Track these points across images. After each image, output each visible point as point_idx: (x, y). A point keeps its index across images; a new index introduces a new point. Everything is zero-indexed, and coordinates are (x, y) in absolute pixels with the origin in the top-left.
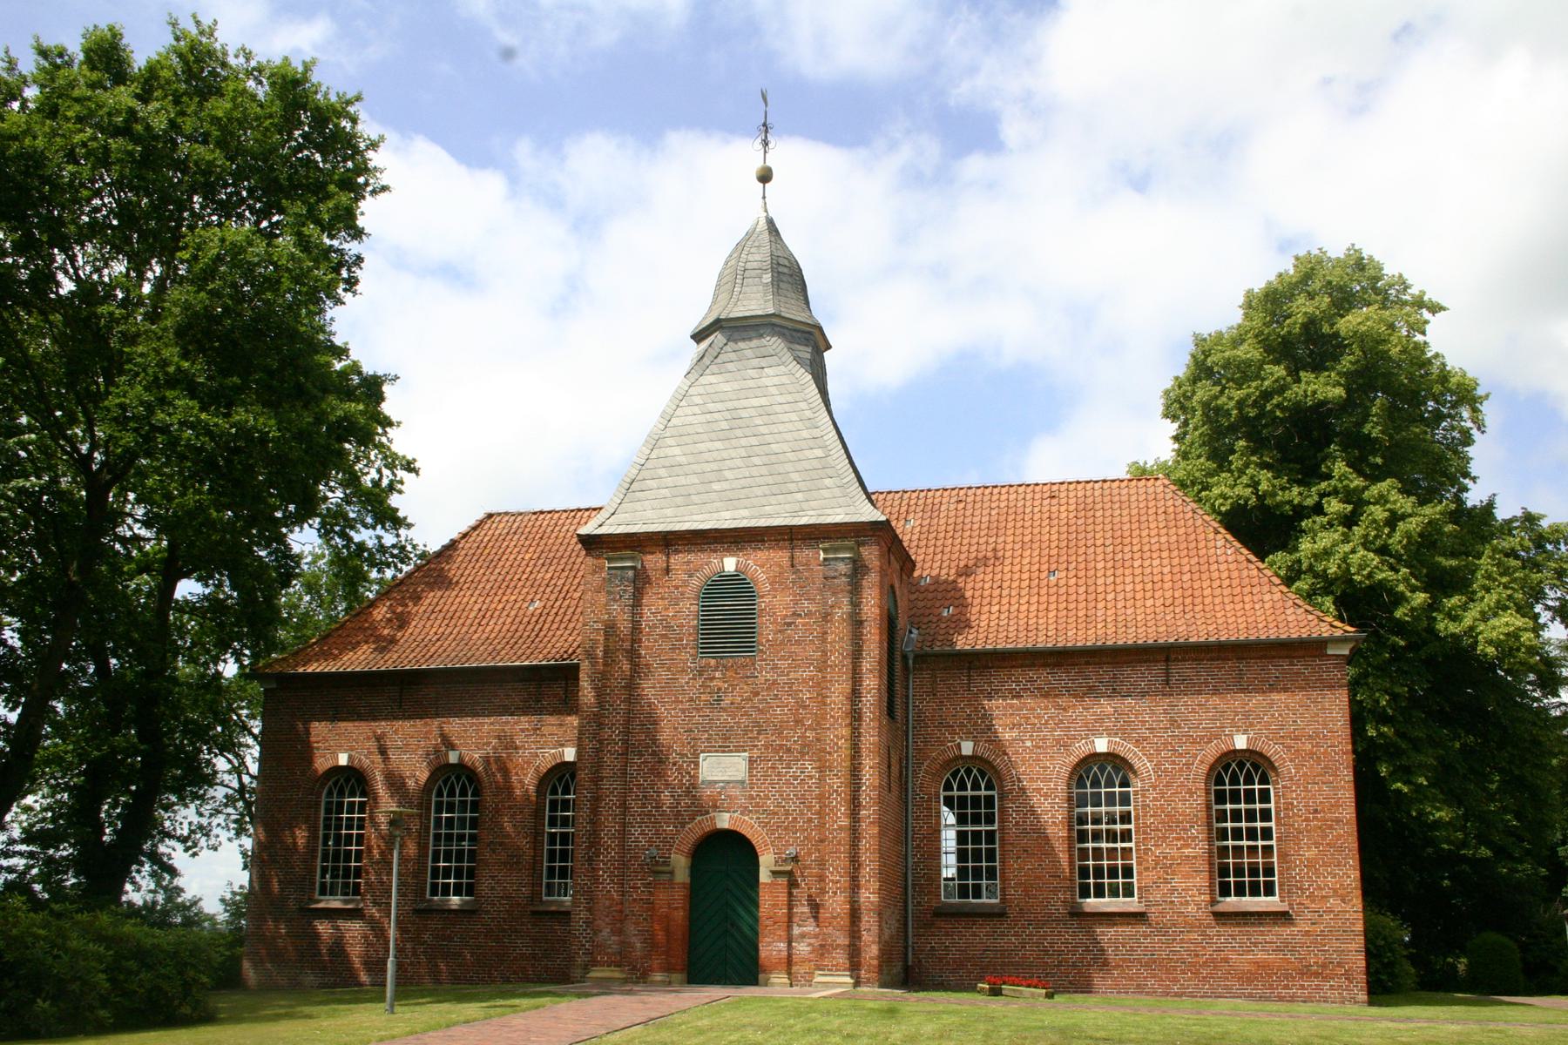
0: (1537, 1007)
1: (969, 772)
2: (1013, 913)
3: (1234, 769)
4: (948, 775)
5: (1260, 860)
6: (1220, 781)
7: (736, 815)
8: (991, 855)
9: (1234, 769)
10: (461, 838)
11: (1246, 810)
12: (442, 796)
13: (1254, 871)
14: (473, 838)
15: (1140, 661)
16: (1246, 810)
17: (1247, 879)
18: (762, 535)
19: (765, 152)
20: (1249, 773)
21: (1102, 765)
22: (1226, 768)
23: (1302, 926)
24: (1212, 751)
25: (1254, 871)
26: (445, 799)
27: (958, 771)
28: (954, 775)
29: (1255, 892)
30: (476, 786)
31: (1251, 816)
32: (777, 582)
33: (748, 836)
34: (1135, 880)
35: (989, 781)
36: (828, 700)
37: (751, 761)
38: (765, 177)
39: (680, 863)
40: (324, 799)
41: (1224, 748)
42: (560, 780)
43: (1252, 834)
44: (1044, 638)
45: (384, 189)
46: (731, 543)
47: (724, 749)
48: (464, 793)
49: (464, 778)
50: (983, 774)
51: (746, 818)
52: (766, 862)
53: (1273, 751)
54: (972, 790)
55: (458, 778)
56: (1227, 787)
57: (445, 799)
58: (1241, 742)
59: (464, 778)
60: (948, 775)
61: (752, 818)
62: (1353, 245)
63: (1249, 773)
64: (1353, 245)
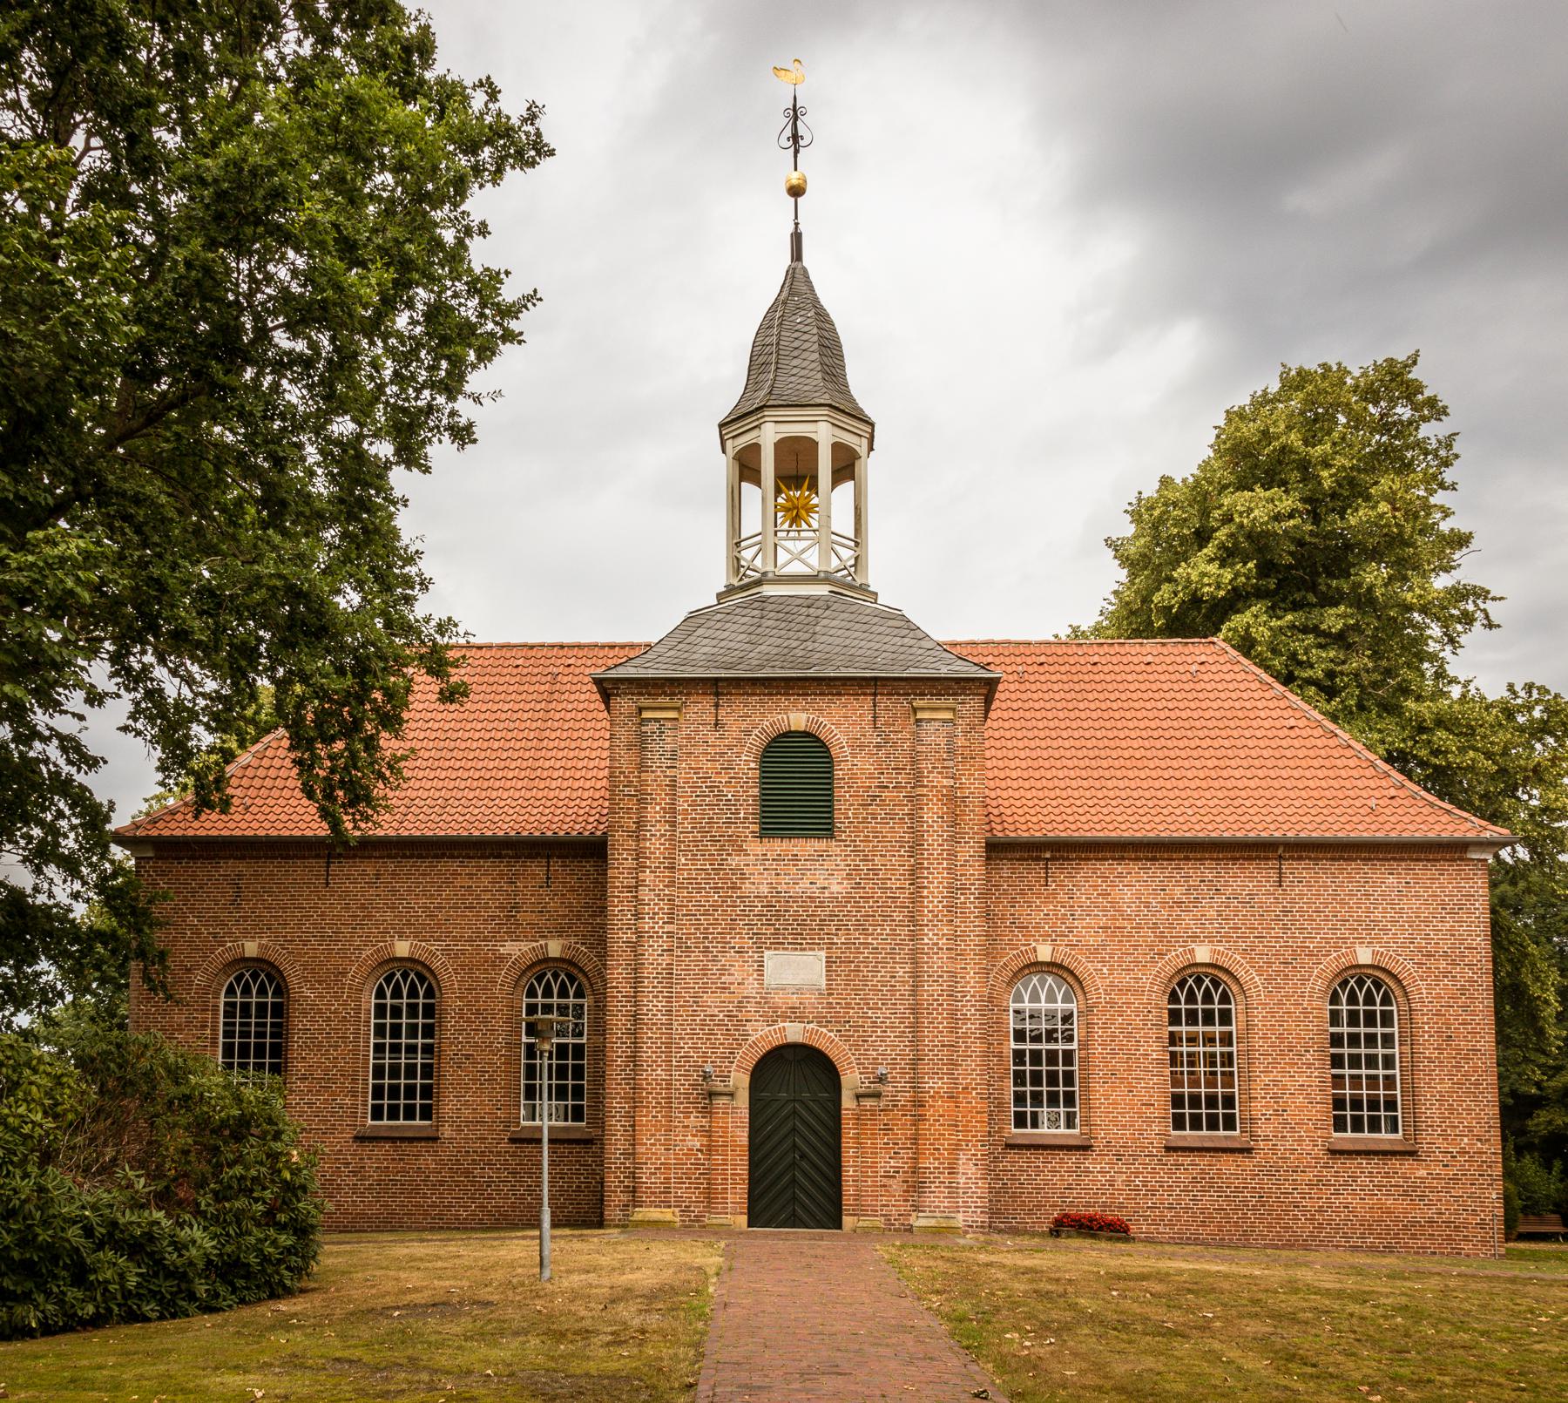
3: (1352, 987)
4: (232, 978)
5: (1381, 1092)
6: (1174, 998)
7: (811, 1025)
9: (1352, 987)
10: (411, 1049)
11: (1349, 1034)
14: (428, 1049)
15: (1250, 859)
16: (1349, 1034)
19: (796, 152)
20: (247, 985)
22: (1345, 983)
24: (1331, 964)
26: (421, 1001)
27: (393, 975)
29: (1375, 1126)
30: (278, 984)
31: (1371, 1040)
32: (858, 746)
34: (1237, 1111)
38: (796, 191)
39: (740, 1080)
42: (539, 980)
43: (1371, 1061)
45: (1216, 428)
46: (799, 695)
47: (798, 946)
48: (262, 991)
49: (412, 975)
50: (572, 979)
51: (824, 1030)
52: (852, 1079)
53: (1405, 967)
55: (556, 976)
56: (1183, 1006)
57: (389, 1001)
58: (1364, 956)
59: (412, 975)
60: (232, 978)
61: (832, 1031)
63: (1369, 994)
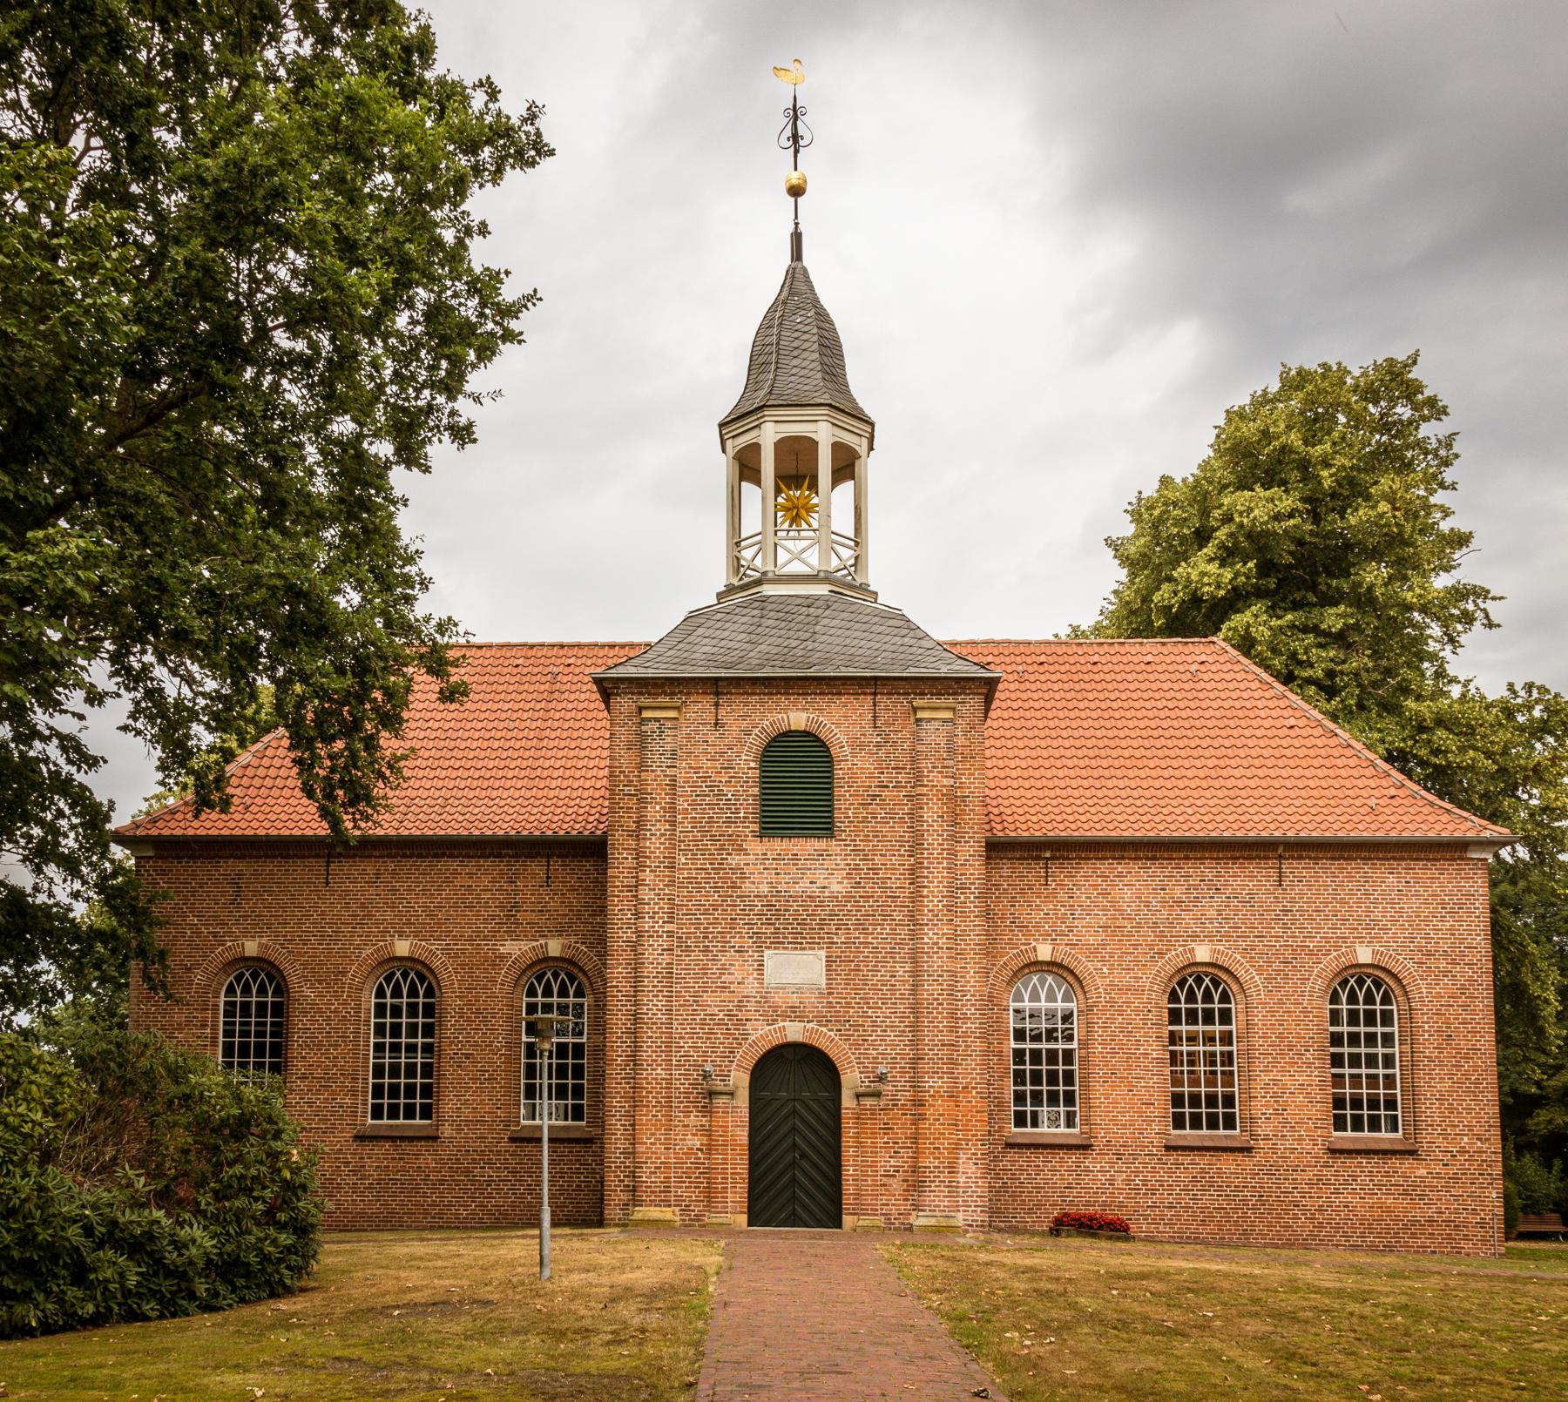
3: (1352, 986)
4: (232, 978)
5: (1381, 1091)
6: (1174, 997)
9: (1352, 986)
10: (411, 1048)
11: (1349, 1033)
13: (1374, 1103)
14: (428, 1049)
15: (1250, 858)
16: (1349, 1033)
17: (1204, 1110)
18: (663, 685)
19: (796, 152)
20: (247, 984)
21: (1360, 978)
22: (1345, 982)
24: (1331, 963)
25: (1374, 1103)
26: (421, 1000)
27: (393, 974)
29: (1375, 1125)
30: (278, 983)
31: (1371, 1039)
32: (858, 746)
34: (1237, 1110)
38: (796, 191)
42: (539, 979)
43: (1371, 1061)
46: (799, 694)
47: (798, 945)
48: (262, 991)
49: (412, 974)
50: (572, 978)
51: (824, 1029)
52: (852, 1079)
53: (1405, 966)
56: (1183, 1006)
57: (389, 1000)
58: (1364, 955)
59: (412, 974)
60: (232, 978)
61: (832, 1030)
62: (484, 230)
63: (1369, 993)
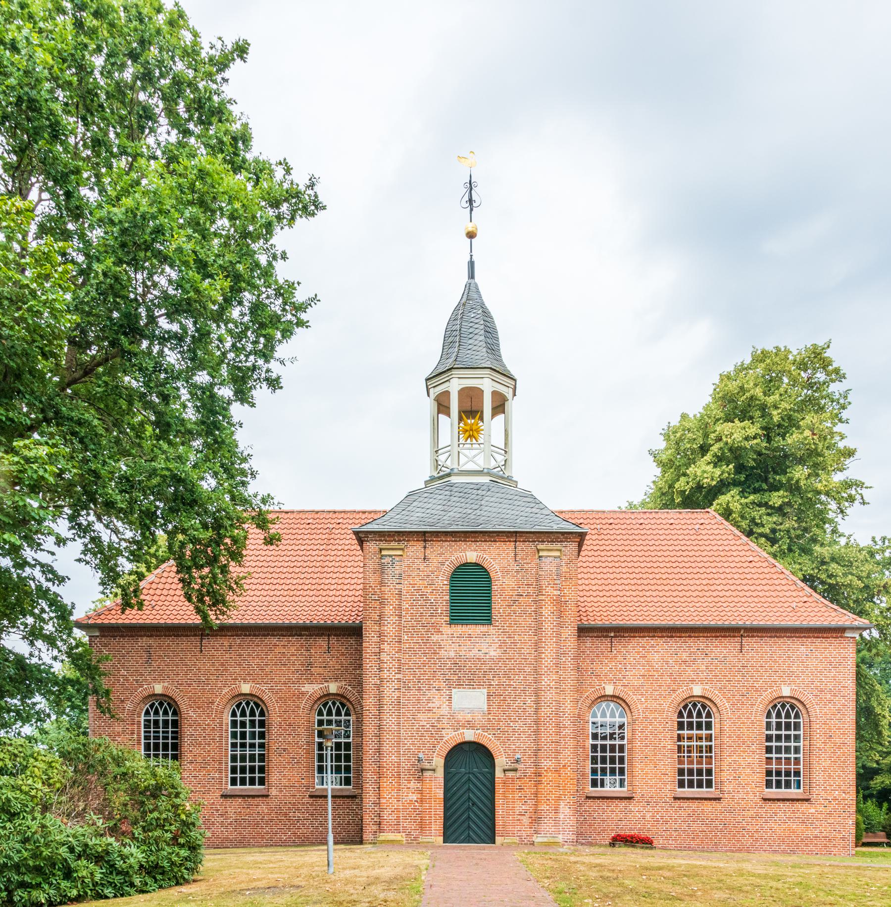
0: (200, 880)
1: (248, 704)
2: (637, 796)
8: (622, 760)
10: (252, 746)
12: (790, 718)
19: (471, 210)
23: (724, 803)
26: (257, 718)
28: (325, 705)
33: (454, 744)
35: (175, 710)
36: (543, 656)
37: (489, 696)
38: (471, 235)
40: (143, 718)
41: (775, 695)
44: (656, 622)
47: (471, 686)
54: (620, 717)
62: (284, 257)
63: (788, 712)
64: (284, 257)
